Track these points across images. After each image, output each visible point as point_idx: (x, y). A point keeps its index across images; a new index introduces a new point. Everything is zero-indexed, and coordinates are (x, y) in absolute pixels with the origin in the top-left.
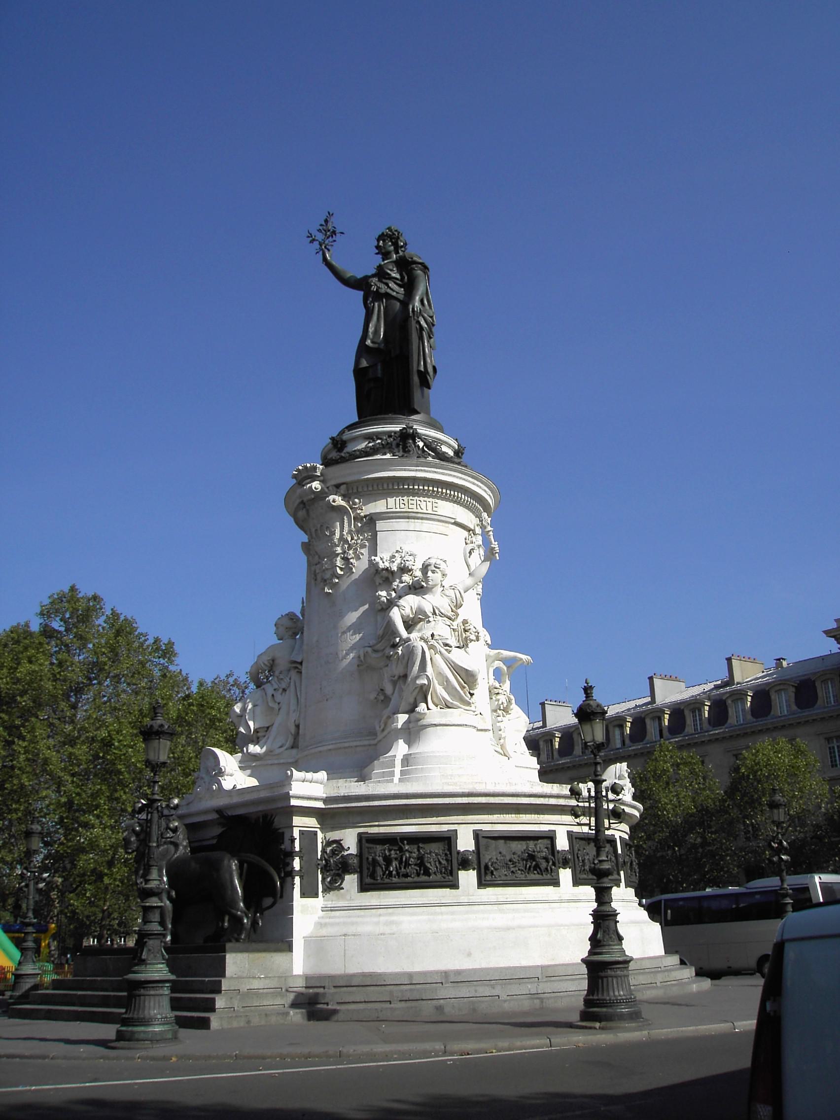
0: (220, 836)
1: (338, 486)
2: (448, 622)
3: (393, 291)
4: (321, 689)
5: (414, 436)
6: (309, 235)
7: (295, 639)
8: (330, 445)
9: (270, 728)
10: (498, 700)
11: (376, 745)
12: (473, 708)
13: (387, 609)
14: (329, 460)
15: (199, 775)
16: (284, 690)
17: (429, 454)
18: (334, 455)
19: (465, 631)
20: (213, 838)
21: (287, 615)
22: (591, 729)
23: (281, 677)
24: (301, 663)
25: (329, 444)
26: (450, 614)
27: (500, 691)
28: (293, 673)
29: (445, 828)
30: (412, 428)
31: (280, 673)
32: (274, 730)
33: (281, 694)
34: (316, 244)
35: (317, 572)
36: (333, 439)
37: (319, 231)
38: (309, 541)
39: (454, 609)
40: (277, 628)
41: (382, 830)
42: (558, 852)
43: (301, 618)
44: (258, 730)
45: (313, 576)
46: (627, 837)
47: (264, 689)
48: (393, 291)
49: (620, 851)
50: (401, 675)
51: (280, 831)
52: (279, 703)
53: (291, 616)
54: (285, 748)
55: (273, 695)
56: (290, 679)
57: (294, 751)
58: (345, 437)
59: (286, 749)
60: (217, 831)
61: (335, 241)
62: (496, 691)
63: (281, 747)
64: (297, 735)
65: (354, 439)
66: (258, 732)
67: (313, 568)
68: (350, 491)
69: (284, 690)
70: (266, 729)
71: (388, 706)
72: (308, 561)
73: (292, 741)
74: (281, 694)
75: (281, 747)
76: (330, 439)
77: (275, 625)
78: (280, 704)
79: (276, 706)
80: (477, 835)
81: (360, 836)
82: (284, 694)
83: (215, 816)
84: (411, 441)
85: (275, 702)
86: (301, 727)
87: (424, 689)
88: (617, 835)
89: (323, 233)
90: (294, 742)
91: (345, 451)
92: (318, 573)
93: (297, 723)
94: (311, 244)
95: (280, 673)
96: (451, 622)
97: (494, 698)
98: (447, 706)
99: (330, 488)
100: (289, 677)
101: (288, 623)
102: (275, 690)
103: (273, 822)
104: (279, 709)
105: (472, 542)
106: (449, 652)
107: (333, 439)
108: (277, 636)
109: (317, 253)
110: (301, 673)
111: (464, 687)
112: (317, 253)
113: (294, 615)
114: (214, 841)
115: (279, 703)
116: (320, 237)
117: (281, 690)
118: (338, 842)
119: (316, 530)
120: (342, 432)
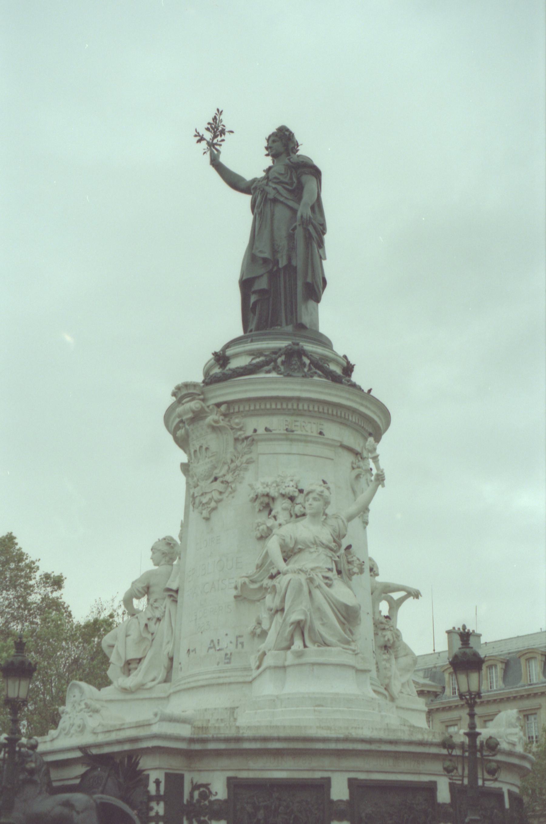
0: (83, 776)
1: (218, 405)
2: (330, 554)
3: (282, 196)
4: (196, 619)
5: (301, 353)
6: (197, 134)
7: (172, 565)
8: (213, 361)
9: (142, 660)
10: (384, 636)
11: (251, 682)
12: (353, 647)
13: (267, 537)
14: (211, 376)
15: (64, 710)
16: (159, 620)
17: (316, 373)
18: (217, 370)
19: (349, 562)
20: (76, 778)
21: (165, 539)
22: (477, 679)
23: (156, 605)
24: (177, 591)
25: (211, 360)
26: (333, 545)
27: (387, 627)
28: (168, 602)
29: (318, 775)
30: (298, 344)
31: (155, 602)
32: (145, 663)
33: (155, 624)
34: (204, 144)
35: (196, 495)
36: (215, 354)
37: (208, 129)
38: (189, 462)
39: (337, 539)
40: (154, 553)
41: (251, 775)
42: (439, 805)
43: (179, 542)
44: (130, 662)
45: (191, 499)
46: (516, 790)
47: (137, 618)
48: (282, 196)
49: (507, 806)
50: (279, 609)
51: (146, 773)
52: (152, 634)
53: (169, 542)
54: (157, 681)
55: (146, 625)
56: (165, 608)
57: (166, 685)
58: (229, 352)
59: (159, 683)
60: (80, 770)
61: (223, 140)
62: (382, 626)
63: (153, 680)
64: (170, 669)
65: (237, 355)
66: (129, 664)
67: (192, 491)
68: (232, 411)
69: (159, 620)
70: (138, 661)
71: (264, 642)
72: (187, 483)
73: (165, 674)
74: (155, 624)
75: (153, 680)
76: (213, 354)
77: (152, 549)
78: (154, 635)
79: (149, 636)
80: (352, 784)
81: (229, 780)
82: (158, 623)
83: (78, 754)
84: (296, 359)
85: (149, 632)
86: (174, 660)
87: (302, 625)
88: (505, 789)
89: (211, 132)
90: (167, 676)
91: (227, 368)
92: (197, 497)
93: (170, 655)
94: (199, 143)
95: (155, 602)
96: (334, 554)
97: (380, 634)
98: (325, 643)
99: (211, 407)
100: (164, 605)
101: (165, 548)
102: (149, 619)
103: (138, 763)
104: (153, 640)
105: (359, 467)
106: (329, 586)
107: (215, 354)
108: (153, 561)
109: (205, 153)
110: (176, 601)
111: (344, 624)
112: (205, 153)
113: (172, 539)
114: (78, 781)
115: (152, 634)
116: (208, 136)
117: (155, 620)
118: (206, 786)
119: (195, 451)
120: (228, 346)
